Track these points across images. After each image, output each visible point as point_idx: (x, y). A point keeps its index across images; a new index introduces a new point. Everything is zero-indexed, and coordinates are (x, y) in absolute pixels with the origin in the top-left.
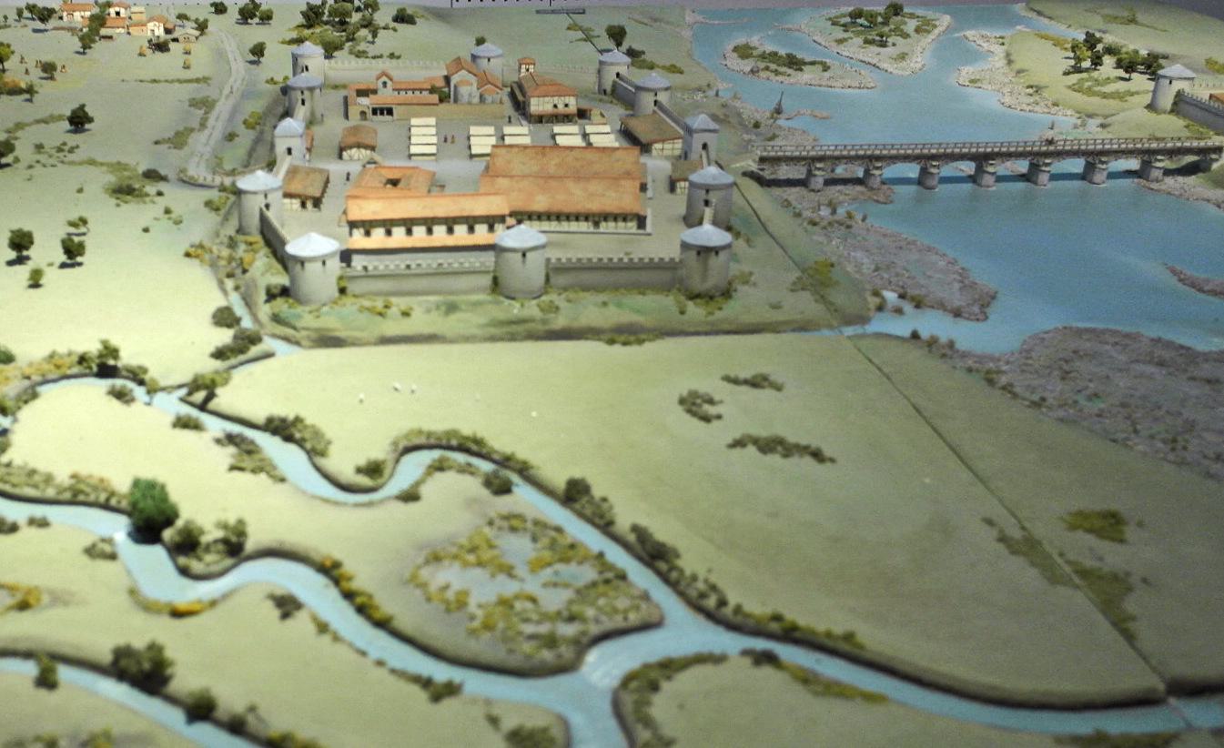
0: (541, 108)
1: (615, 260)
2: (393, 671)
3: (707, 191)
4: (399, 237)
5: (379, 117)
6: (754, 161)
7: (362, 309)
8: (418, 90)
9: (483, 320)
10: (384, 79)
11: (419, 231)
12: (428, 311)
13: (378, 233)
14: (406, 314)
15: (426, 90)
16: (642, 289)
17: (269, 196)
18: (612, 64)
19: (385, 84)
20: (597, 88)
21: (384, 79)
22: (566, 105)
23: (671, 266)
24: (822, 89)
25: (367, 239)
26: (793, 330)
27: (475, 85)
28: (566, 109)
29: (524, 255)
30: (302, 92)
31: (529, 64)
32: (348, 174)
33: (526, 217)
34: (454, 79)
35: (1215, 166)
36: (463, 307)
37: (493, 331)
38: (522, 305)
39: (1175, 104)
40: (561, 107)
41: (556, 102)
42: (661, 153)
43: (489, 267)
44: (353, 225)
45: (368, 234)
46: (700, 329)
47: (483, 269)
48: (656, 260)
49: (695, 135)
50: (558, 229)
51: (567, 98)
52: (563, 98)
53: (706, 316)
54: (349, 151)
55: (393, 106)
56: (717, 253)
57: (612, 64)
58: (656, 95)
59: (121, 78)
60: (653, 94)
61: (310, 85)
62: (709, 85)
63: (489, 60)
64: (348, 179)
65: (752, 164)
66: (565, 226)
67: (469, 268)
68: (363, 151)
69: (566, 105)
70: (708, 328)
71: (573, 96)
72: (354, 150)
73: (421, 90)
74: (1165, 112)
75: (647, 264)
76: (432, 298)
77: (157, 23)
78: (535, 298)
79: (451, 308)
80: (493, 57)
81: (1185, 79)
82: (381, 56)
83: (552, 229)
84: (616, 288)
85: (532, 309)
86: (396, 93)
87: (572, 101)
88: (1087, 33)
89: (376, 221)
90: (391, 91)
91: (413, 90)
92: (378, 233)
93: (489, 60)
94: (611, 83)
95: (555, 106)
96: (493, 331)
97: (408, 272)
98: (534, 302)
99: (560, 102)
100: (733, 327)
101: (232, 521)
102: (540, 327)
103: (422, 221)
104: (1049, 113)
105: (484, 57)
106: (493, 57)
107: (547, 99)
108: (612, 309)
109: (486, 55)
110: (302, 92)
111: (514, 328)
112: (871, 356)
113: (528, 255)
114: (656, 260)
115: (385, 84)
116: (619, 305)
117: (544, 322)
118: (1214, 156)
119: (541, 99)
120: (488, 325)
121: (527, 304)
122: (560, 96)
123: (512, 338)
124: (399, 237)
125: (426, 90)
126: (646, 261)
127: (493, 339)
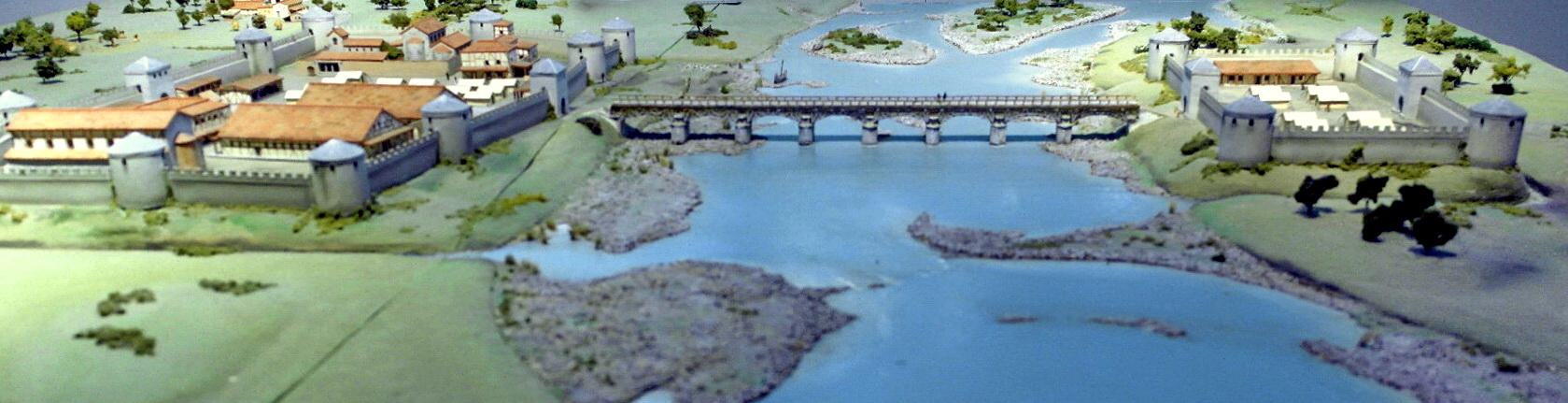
0: (473, 65)
1: (238, 174)
3: (430, 119)
4: (60, 149)
6: (606, 109)
8: (368, 46)
9: (86, 229)
10: (334, 35)
11: (80, 143)
12: (41, 218)
13: (60, 143)
16: (273, 206)
17: (10, 116)
21: (334, 35)
22: (498, 62)
23: (300, 184)
24: (867, 64)
25: (51, 150)
26: (406, 254)
28: (498, 66)
29: (124, 162)
30: (243, 45)
33: (263, 145)
37: (94, 240)
40: (492, 63)
41: (487, 59)
43: (105, 175)
44: (16, 134)
45: (29, 144)
46: (305, 248)
47: (99, 178)
48: (294, 176)
50: (293, 157)
51: (498, 54)
56: (332, 168)
58: (581, 51)
59: (171, 46)
60: (577, 49)
61: (251, 38)
62: (945, 96)
63: (482, 25)
65: (604, 112)
67: (85, 176)
69: (498, 62)
71: (504, 52)
73: (371, 47)
74: (1156, 81)
75: (285, 180)
78: (146, 210)
79: (65, 216)
80: (486, 23)
86: (347, 49)
88: (1193, 14)
89: (36, 131)
90: (342, 48)
91: (364, 47)
92: (40, 143)
93: (482, 25)
95: (487, 63)
96: (94, 240)
97: (22, 178)
99: (492, 59)
100: (343, 247)
102: (142, 239)
103: (80, 133)
104: (1068, 86)
105: (478, 22)
107: (478, 55)
110: (243, 45)
112: (301, 248)
113: (130, 162)
114: (283, 176)
115: (335, 40)
116: (236, 222)
117: (146, 233)
118: (1131, 117)
119: (472, 55)
120: (90, 235)
121: (134, 214)
123: (112, 247)
124: (60, 149)
126: (272, 176)
127: (91, 247)
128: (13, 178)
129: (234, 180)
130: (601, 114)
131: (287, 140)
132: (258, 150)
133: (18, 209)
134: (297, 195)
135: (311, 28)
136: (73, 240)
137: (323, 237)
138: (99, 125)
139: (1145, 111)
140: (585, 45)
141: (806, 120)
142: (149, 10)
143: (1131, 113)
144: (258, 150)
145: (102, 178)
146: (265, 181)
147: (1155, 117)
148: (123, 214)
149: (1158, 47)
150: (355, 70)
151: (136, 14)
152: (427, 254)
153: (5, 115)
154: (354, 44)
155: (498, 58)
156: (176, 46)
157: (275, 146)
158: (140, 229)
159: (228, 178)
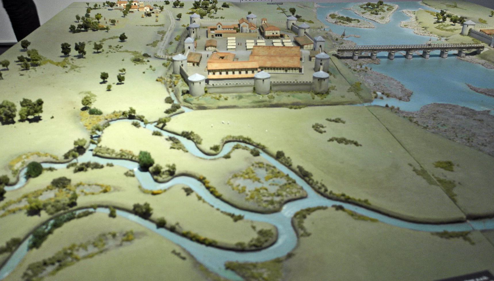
0: (269, 34)
2: (222, 212)
3: (321, 60)
4: (224, 75)
5: (218, 37)
6: (336, 51)
7: (212, 98)
9: (250, 101)
10: (219, 25)
12: (233, 98)
14: (226, 99)
15: (232, 28)
16: (300, 91)
18: (291, 20)
19: (219, 27)
20: (286, 28)
21: (219, 25)
22: (277, 33)
23: (310, 84)
24: (357, 28)
27: (248, 27)
28: (277, 34)
29: (263, 81)
30: (193, 29)
31: (265, 20)
32: (208, 55)
34: (241, 25)
35: (482, 52)
36: (244, 97)
38: (263, 96)
39: (469, 33)
40: (275, 34)
41: (273, 32)
42: (306, 48)
44: (209, 71)
45: (214, 74)
47: (250, 85)
49: (317, 43)
50: (274, 72)
51: (277, 31)
52: (275, 31)
53: (321, 100)
54: (208, 48)
55: (222, 34)
56: (324, 80)
57: (291, 20)
58: (305, 30)
60: (304, 30)
61: (196, 27)
63: (252, 19)
64: (208, 57)
65: (336, 52)
66: (276, 71)
68: (212, 48)
69: (277, 33)
70: (321, 104)
71: (279, 30)
72: (210, 47)
73: (231, 29)
74: (466, 35)
76: (234, 94)
77: (147, 7)
78: (267, 94)
79: (240, 97)
80: (254, 18)
81: (471, 25)
82: (218, 18)
83: (272, 72)
84: (292, 91)
85: (266, 98)
86: (223, 29)
87: (278, 32)
88: (441, 11)
89: (217, 70)
90: (221, 29)
91: (228, 29)
92: (217, 74)
93: (252, 19)
94: (291, 26)
95: (273, 34)
97: (227, 86)
98: (267, 95)
99: (275, 32)
101: (171, 165)
102: (268, 103)
105: (251, 18)
106: (254, 18)
107: (270, 31)
108: (291, 98)
109: (251, 17)
110: (193, 29)
111: (260, 104)
113: (265, 80)
115: (219, 27)
116: (293, 96)
117: (270, 102)
118: (481, 49)
119: (269, 31)
120: (251, 103)
121: (264, 96)
122: (275, 30)
123: (260, 107)
124: (224, 75)
125: (232, 28)
127: (254, 107)
128: (223, 86)
129: (291, 84)
130: (335, 52)
131: (273, 67)
132: (286, 71)
133: (224, 96)
134: (308, 87)
135: (195, 20)
136: (248, 105)
137: (322, 100)
138: (237, 67)
139: (486, 48)
140: (307, 28)
141: (393, 52)
142: (97, 9)
143: (482, 48)
144: (286, 71)
145: (251, 85)
146: (300, 84)
147: (488, 49)
148: (261, 96)
149: (468, 26)
150: (233, 37)
151: (93, 10)
152: (355, 104)
153: (182, 62)
154: (225, 27)
155: (277, 32)
156: (137, 25)
157: (280, 69)
158: (268, 100)
159: (286, 83)
